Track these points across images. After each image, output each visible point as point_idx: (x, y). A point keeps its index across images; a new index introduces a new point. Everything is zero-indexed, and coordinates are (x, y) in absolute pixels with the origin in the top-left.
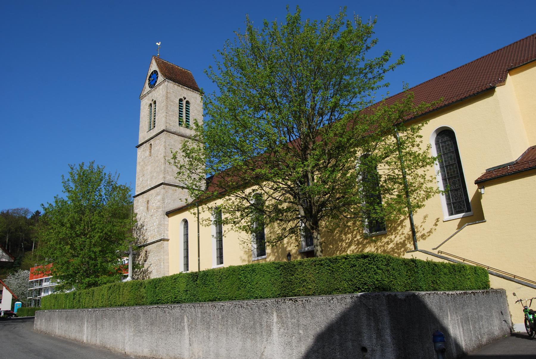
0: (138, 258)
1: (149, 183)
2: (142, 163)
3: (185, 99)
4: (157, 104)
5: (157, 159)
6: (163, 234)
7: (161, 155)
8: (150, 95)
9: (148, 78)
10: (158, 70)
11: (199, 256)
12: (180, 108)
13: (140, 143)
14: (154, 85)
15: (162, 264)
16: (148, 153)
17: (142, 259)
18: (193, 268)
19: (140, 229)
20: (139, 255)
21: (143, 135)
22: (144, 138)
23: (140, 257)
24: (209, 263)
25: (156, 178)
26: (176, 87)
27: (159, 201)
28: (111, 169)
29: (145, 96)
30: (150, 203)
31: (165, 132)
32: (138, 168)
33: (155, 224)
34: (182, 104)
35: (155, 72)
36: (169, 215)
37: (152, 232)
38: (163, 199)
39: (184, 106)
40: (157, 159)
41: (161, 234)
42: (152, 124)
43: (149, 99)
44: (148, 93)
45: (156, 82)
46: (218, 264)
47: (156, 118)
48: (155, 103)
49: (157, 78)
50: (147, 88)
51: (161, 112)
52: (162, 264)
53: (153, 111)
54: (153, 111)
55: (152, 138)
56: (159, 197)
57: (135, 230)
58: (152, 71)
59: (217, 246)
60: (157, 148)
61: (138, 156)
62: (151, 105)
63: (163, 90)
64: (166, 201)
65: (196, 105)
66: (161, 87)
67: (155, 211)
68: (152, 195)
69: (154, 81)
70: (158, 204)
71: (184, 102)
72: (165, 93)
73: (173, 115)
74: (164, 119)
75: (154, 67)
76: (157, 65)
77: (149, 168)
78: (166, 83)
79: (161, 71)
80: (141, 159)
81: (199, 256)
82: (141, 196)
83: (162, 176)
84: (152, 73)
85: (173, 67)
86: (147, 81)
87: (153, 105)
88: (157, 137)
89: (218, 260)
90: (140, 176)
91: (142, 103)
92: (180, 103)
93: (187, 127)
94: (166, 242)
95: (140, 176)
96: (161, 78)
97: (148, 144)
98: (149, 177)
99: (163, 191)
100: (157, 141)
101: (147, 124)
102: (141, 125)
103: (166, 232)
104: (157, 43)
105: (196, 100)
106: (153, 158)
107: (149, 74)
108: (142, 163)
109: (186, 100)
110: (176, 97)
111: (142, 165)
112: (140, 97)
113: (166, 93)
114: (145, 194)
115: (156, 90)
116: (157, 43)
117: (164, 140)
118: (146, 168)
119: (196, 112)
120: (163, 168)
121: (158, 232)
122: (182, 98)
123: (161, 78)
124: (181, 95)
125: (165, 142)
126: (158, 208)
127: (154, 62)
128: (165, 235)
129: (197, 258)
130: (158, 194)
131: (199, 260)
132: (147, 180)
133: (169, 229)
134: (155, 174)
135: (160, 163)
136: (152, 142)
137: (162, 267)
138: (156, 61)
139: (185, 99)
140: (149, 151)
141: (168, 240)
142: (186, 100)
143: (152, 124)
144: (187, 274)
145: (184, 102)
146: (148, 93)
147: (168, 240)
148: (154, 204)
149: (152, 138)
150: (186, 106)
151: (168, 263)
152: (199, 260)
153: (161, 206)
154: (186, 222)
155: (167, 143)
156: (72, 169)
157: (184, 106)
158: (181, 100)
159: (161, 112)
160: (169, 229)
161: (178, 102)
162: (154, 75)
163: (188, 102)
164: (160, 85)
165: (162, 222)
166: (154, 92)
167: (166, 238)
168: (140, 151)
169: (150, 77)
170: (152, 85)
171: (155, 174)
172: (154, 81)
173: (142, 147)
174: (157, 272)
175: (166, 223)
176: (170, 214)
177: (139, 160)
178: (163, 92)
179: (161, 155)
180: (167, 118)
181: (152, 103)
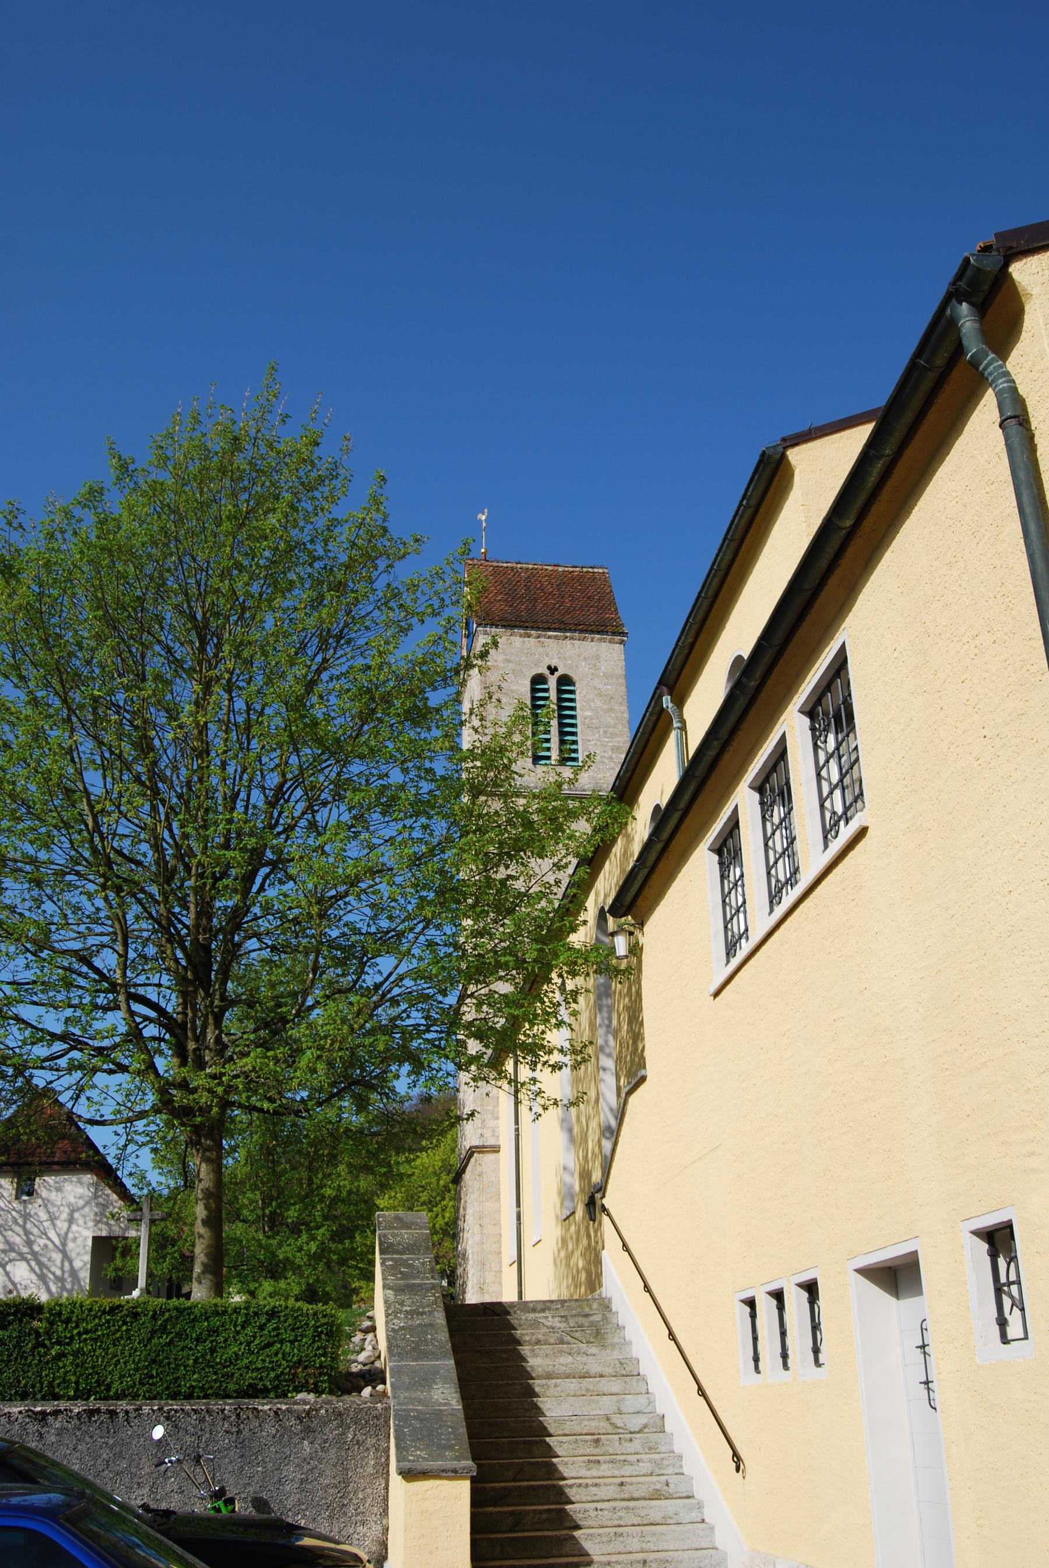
11: (518, 1205)
81: (518, 1205)
94: (489, 1157)
128: (488, 1133)
139: (553, 670)
142: (557, 674)
167: (491, 1142)
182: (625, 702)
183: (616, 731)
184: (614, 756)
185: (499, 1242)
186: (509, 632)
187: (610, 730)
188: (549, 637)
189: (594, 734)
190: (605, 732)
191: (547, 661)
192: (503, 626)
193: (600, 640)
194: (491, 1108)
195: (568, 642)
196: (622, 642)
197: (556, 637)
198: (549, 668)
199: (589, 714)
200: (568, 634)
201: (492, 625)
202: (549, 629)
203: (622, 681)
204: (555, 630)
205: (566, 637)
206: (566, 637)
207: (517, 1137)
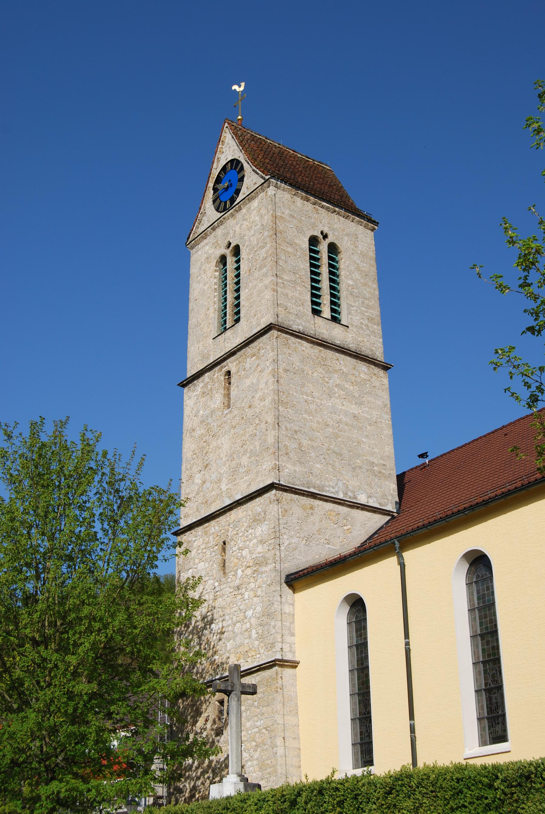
0: (195, 723)
1: (224, 487)
2: (199, 432)
3: (325, 237)
4: (244, 254)
5: (249, 413)
6: (278, 646)
7: (263, 399)
8: (219, 231)
9: (211, 185)
10: (241, 157)
11: (412, 716)
12: (312, 265)
13: (191, 371)
14: (233, 200)
15: (279, 741)
16: (218, 398)
17: (209, 726)
18: (390, 759)
19: (199, 633)
20: (198, 713)
21: (202, 343)
22: (205, 357)
23: (201, 722)
24: (453, 741)
25: (248, 472)
26: (299, 201)
27: (262, 542)
28: (117, 442)
29: (204, 235)
30: (232, 548)
31: (274, 333)
32: (189, 446)
33: (249, 613)
34: (317, 252)
35: (235, 164)
36: (296, 584)
37: (238, 640)
38: (277, 534)
39: (322, 257)
40: (249, 413)
41: (273, 645)
42: (230, 313)
43: (216, 245)
44: (213, 227)
45: (238, 192)
46: (483, 743)
47: (243, 293)
48: (237, 251)
49: (241, 180)
50: (209, 212)
51: (257, 274)
52: (279, 741)
53: (231, 275)
54: (231, 275)
55: (232, 354)
56: (262, 530)
57: (180, 634)
58: (223, 162)
59: (476, 680)
60: (248, 382)
61: (187, 411)
62: (223, 259)
63: (263, 211)
64: (285, 540)
65: (355, 257)
66: (255, 204)
67: (249, 571)
68: (236, 524)
69: (232, 191)
70: (260, 549)
71: (323, 248)
72: (267, 219)
73: (295, 282)
74: (268, 295)
75: (229, 149)
76: (241, 143)
77: (225, 443)
78: (271, 190)
79: (253, 160)
80: (197, 420)
81: (412, 716)
82: (199, 530)
83: (268, 464)
84: (224, 169)
85: (281, 153)
86: (210, 194)
87: (230, 260)
88: (248, 350)
89: (481, 729)
90: (195, 469)
91: (193, 259)
92: (311, 250)
93: (335, 319)
94: (288, 672)
95: (195, 469)
96: (252, 179)
97: (218, 374)
98: (223, 469)
99: (274, 509)
100: (249, 362)
101: (213, 315)
102: (192, 321)
103: (288, 639)
104: (235, 87)
105: (357, 242)
106: (236, 412)
107: (215, 173)
108: (199, 432)
109: (328, 241)
110: (300, 230)
111: (201, 437)
112: (188, 242)
113: (270, 222)
114: (213, 523)
115: (239, 215)
116: (235, 87)
117: (271, 355)
118: (214, 444)
119: (356, 275)
120: (271, 440)
121: (261, 637)
122: (317, 234)
123: (252, 179)
124: (314, 226)
125: (276, 361)
126: (260, 563)
127: (228, 137)
128: (286, 648)
129: (407, 722)
130: (257, 520)
131: (412, 730)
132: (220, 480)
133: (298, 627)
134: (245, 460)
135: (263, 426)
136: (231, 365)
137: (280, 751)
138: (235, 134)
139: (325, 237)
140: (222, 391)
141: (294, 665)
142: (328, 241)
143: (230, 313)
144: (493, 773)
145: (323, 248)
146: (213, 227)
147: (294, 665)
148: (245, 552)
149: (232, 354)
150: (330, 258)
151: (297, 738)
152: (412, 730)
153: (269, 555)
154: (356, 605)
155: (282, 366)
156: (10, 437)
157: (322, 257)
158: (313, 241)
159: (257, 274)
160: (297, 631)
161: (305, 245)
162: (233, 174)
163: (333, 249)
164: (250, 200)
165: (276, 606)
166: (231, 222)
167: (288, 657)
168: (192, 397)
169: (218, 180)
170: (227, 198)
171: (245, 460)
172: (232, 191)
173: (199, 384)
174: (261, 769)
175: (287, 609)
176: (297, 580)
177: (189, 421)
178: (262, 217)
179: (263, 399)
180: (274, 290)
181: (228, 252)
182: (376, 281)
183: (370, 304)
184: (370, 325)
185: (299, 756)
186: (294, 191)
187: (366, 301)
188: (322, 207)
189: (355, 302)
190: (363, 303)
191: (321, 228)
192: (290, 185)
193: (359, 222)
194: (288, 624)
195: (335, 216)
196: (373, 230)
197: (327, 209)
198: (322, 233)
199: (351, 282)
200: (337, 209)
201: (282, 181)
202: (324, 200)
203: (373, 262)
204: (328, 202)
205: (335, 211)
206: (335, 211)
207: (408, 652)
